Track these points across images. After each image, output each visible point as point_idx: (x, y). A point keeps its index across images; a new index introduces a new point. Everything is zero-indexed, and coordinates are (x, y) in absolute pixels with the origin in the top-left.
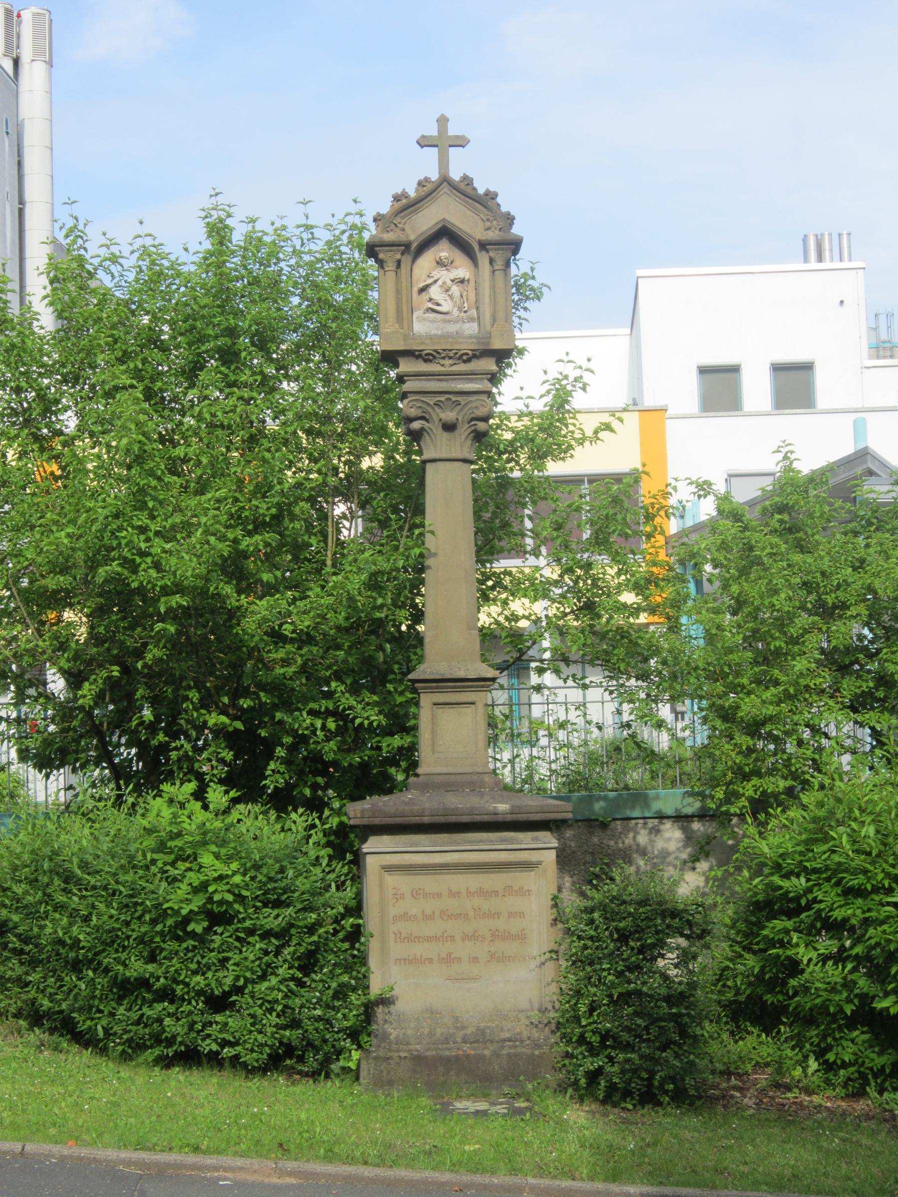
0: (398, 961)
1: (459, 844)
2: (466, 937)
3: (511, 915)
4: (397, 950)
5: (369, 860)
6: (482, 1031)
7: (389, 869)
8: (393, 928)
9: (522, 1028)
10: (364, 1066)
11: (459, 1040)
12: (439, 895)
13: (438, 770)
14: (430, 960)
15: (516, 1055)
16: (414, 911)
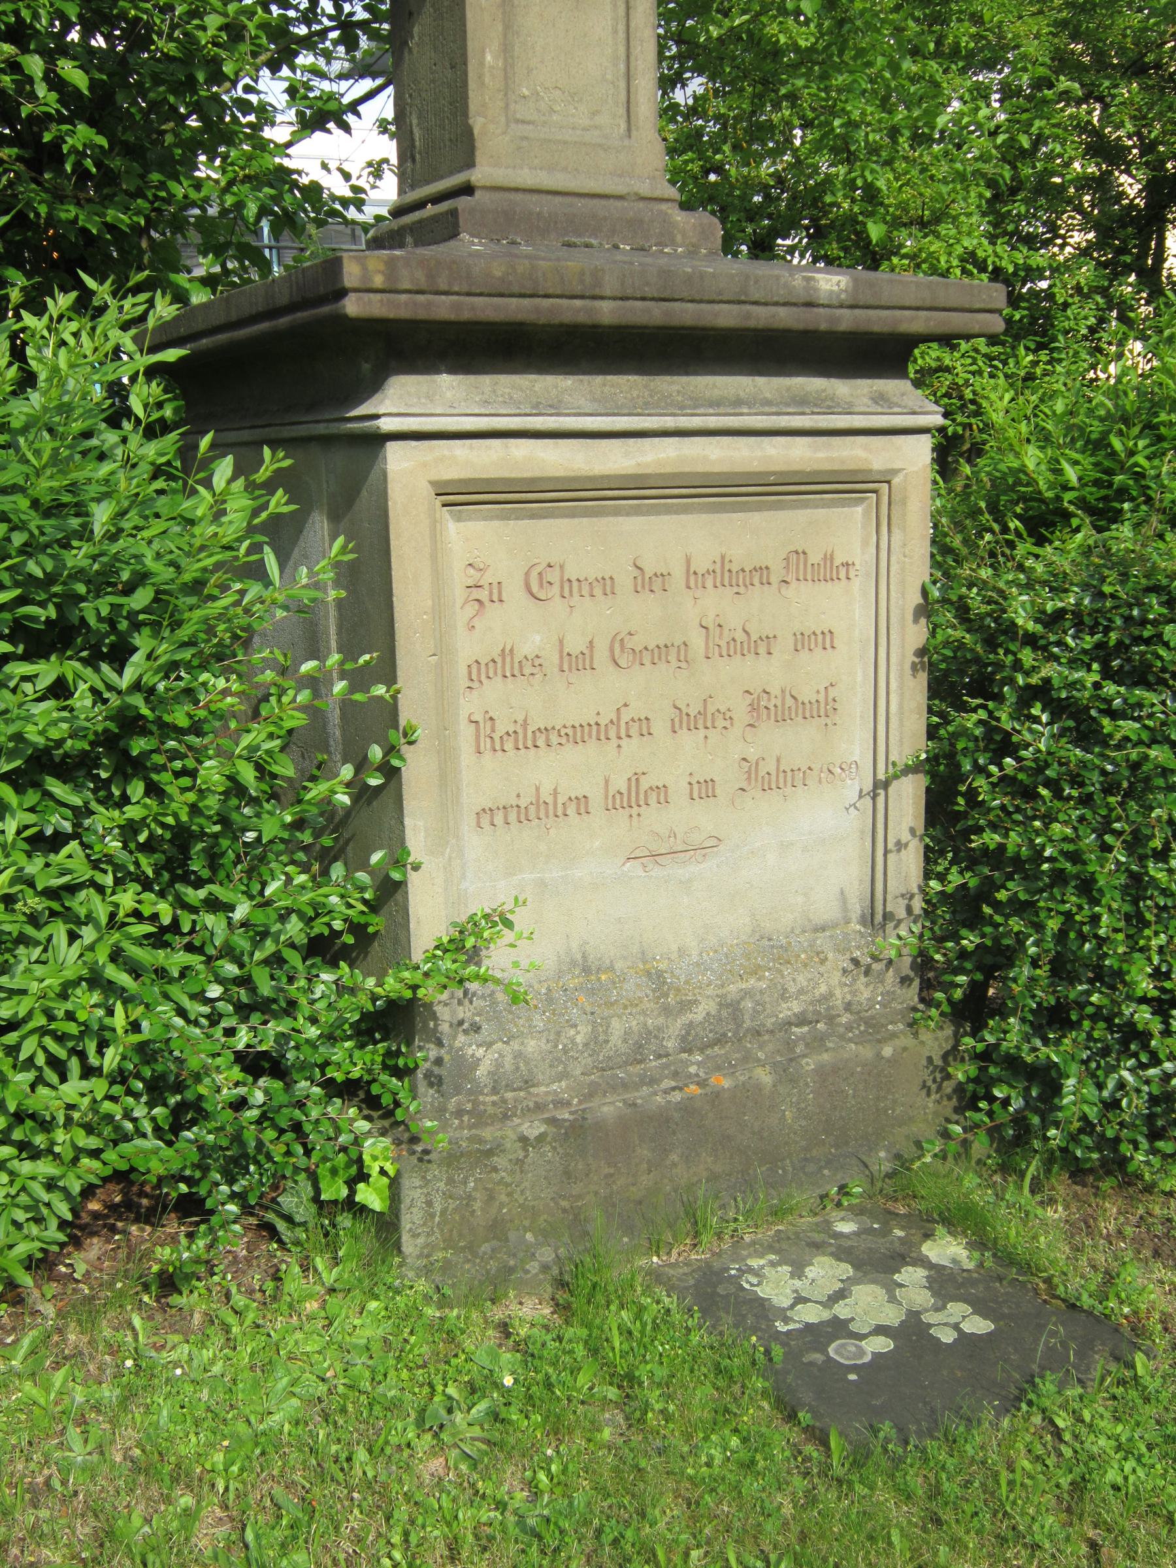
0: (486, 814)
1: (682, 409)
2: (686, 720)
3: (805, 641)
4: (483, 779)
5: (398, 460)
6: (732, 1007)
7: (458, 496)
8: (469, 705)
9: (831, 982)
10: (413, 1191)
11: (670, 1044)
12: (607, 585)
13: (526, 177)
14: (582, 803)
15: (835, 1070)
16: (532, 642)
